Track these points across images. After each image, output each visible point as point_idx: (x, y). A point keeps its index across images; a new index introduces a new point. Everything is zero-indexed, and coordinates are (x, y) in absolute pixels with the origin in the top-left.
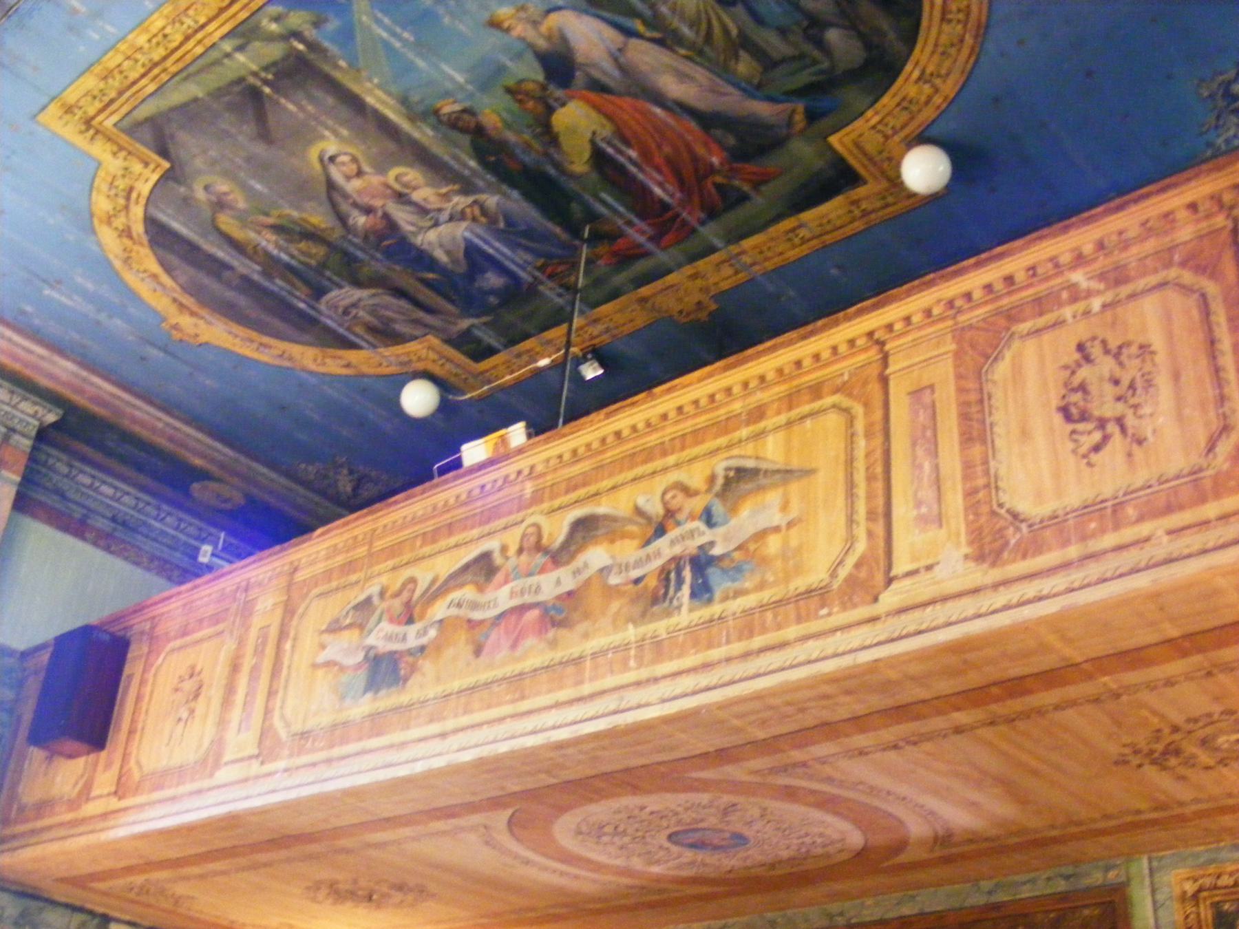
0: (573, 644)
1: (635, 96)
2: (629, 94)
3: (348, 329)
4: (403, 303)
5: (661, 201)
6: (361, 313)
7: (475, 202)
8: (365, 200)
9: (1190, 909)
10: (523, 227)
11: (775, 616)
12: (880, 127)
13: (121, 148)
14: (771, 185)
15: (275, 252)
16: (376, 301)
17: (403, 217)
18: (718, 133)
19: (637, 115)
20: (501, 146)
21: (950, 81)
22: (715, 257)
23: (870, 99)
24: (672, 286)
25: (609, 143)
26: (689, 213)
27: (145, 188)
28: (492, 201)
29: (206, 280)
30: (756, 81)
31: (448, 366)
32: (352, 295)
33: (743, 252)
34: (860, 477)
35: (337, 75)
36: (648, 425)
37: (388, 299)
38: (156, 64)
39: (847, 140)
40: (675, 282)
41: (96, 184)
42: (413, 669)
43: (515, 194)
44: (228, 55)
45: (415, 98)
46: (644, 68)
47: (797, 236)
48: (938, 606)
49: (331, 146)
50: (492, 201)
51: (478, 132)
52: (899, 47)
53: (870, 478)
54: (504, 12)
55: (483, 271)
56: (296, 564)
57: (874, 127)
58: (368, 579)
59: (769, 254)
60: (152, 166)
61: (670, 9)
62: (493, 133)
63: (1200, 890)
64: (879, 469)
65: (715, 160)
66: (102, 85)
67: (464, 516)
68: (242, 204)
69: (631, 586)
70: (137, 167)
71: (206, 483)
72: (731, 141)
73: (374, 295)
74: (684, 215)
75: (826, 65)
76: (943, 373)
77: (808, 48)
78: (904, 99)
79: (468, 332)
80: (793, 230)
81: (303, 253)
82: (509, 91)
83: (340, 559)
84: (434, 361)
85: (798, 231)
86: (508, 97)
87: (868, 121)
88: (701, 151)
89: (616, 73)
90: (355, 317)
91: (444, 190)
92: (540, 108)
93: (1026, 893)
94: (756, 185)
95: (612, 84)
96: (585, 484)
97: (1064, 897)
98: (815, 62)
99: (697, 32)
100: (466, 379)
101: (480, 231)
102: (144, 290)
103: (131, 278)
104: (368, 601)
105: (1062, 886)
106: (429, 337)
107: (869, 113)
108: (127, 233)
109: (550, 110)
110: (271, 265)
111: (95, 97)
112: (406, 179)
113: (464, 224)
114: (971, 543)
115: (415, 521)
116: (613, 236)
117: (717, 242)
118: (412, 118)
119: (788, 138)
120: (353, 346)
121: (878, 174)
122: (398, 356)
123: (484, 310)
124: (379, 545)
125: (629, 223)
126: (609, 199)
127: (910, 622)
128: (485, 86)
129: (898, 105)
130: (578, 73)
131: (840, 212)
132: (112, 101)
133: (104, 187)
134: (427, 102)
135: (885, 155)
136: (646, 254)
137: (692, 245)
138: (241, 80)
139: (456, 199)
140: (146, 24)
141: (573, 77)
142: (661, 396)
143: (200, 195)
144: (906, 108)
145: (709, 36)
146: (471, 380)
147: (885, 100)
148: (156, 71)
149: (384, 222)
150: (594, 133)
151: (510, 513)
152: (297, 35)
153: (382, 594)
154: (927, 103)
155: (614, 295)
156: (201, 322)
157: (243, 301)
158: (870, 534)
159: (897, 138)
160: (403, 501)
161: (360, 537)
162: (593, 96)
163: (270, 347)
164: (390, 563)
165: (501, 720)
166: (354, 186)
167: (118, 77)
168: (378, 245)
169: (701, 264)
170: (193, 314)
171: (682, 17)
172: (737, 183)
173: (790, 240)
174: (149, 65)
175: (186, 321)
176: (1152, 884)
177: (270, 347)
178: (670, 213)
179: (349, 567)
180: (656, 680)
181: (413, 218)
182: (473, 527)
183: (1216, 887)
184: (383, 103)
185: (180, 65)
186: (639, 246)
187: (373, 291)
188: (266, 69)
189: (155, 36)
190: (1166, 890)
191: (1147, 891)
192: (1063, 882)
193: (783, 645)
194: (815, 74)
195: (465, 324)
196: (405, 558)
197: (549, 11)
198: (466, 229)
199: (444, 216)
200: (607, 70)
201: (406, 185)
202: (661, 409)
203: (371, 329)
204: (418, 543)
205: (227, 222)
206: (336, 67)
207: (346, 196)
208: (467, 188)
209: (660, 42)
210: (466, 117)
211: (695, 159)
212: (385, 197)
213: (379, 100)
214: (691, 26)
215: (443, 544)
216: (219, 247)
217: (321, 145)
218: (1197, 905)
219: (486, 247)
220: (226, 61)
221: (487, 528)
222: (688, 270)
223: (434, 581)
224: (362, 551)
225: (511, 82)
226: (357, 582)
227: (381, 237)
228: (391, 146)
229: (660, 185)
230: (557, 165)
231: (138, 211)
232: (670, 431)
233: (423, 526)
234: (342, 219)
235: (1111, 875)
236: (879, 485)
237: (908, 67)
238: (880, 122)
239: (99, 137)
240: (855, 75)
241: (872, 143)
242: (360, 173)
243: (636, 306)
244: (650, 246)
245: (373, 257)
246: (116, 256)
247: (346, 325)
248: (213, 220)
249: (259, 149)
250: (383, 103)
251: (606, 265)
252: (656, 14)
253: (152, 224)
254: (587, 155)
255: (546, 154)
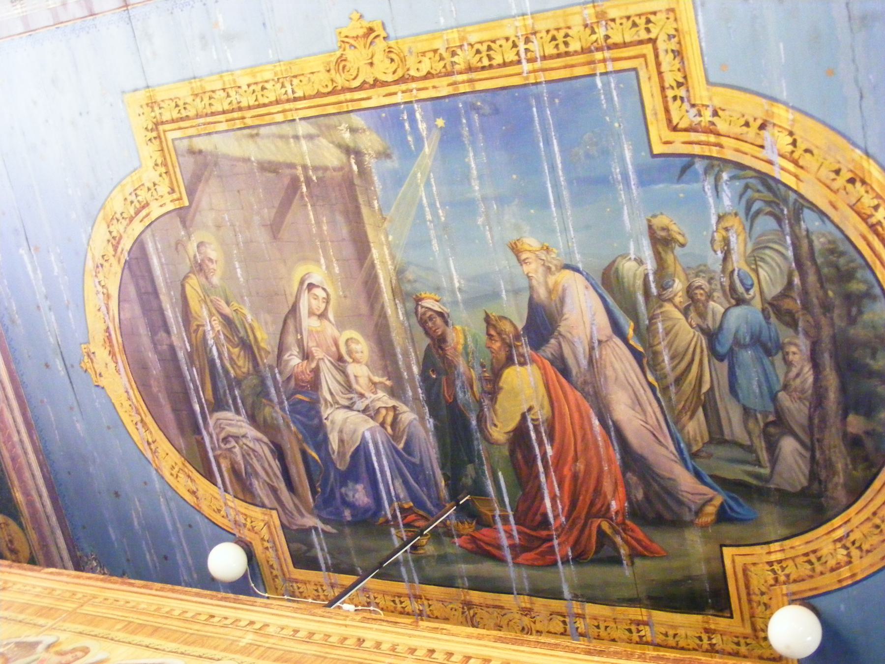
1: (586, 395)
2: (582, 391)
3: (216, 458)
4: (275, 465)
5: (545, 515)
6: (237, 450)
7: (394, 408)
8: (310, 344)
10: (417, 461)
12: (776, 567)
13: (165, 165)
14: (648, 563)
15: (211, 342)
16: (257, 447)
17: (329, 381)
18: (633, 479)
19: (576, 416)
20: (449, 367)
21: (868, 559)
22: (556, 605)
23: (783, 531)
24: (502, 608)
25: (536, 428)
26: (559, 544)
27: (156, 211)
28: (408, 416)
29: (143, 331)
30: (695, 449)
31: (271, 553)
32: (241, 427)
33: (582, 616)
35: (365, 211)
36: (393, 649)
37: (266, 451)
38: (240, 109)
39: (740, 561)
40: (507, 606)
41: (124, 182)
43: (430, 423)
44: (296, 137)
45: (410, 275)
46: (609, 372)
47: (639, 631)
49: (317, 275)
50: (408, 416)
51: (439, 341)
52: (841, 495)
54: (531, 242)
55: (357, 481)
56: (10, 585)
57: (770, 563)
58: (52, 628)
59: (603, 633)
60: (175, 196)
61: (665, 329)
62: (450, 353)
65: (614, 505)
66: (189, 100)
67: (174, 628)
68: (215, 280)
70: (164, 189)
71: (10, 521)
72: (640, 495)
73: (258, 440)
74: (556, 542)
75: (765, 471)
77: (760, 445)
78: (814, 552)
79: (307, 531)
80: (638, 623)
81: (231, 359)
82: (488, 319)
83: (46, 602)
84: (263, 539)
85: (641, 627)
86: (484, 325)
87: (769, 553)
88: (607, 486)
89: (584, 362)
90: (230, 450)
91: (376, 379)
92: (503, 355)
94: (634, 554)
95: (574, 371)
98: (758, 463)
99: (674, 368)
100: (276, 576)
101: (379, 439)
102: (93, 301)
103: (90, 284)
104: (33, 646)
106: (274, 513)
107: (775, 546)
108: (115, 242)
109: (509, 361)
110: (199, 351)
111: (177, 106)
112: (353, 346)
113: (372, 423)
115: (135, 610)
116: (483, 522)
117: (567, 594)
118: (396, 292)
119: (691, 523)
120: (209, 476)
121: (747, 616)
122: (238, 513)
123: (335, 520)
124: (88, 609)
125: (505, 519)
128: (471, 303)
129: (806, 555)
130: (553, 341)
131: (690, 633)
132: (188, 118)
133: (129, 189)
134: (418, 285)
135: (765, 599)
136: (501, 560)
137: (544, 577)
138: (292, 166)
139: (381, 394)
140: (257, 69)
141: (547, 341)
142: (423, 630)
143: (192, 248)
144: (810, 562)
145: (679, 381)
146: (279, 581)
147: (796, 541)
148: (236, 115)
149: (312, 375)
150: (530, 409)
151: (215, 648)
152: (358, 154)
153: (49, 647)
154: (832, 570)
155: (448, 582)
156: (112, 365)
157: (156, 369)
159: (785, 589)
160: (138, 587)
161: (80, 595)
162: (551, 371)
163: (147, 429)
164: (81, 628)
166: (309, 323)
167: (206, 100)
168: (293, 394)
169: (539, 602)
170: (112, 353)
171: (670, 345)
172: (618, 540)
173: (630, 631)
174: (235, 106)
175: (102, 355)
177: (147, 429)
178: (544, 533)
179: (46, 612)
181: (335, 388)
182: (174, 641)
184: (383, 263)
185: (257, 122)
186: (499, 547)
187: (259, 435)
188: (315, 169)
189: (256, 83)
194: (749, 474)
195: (310, 521)
196: (97, 631)
197: (567, 267)
198: (370, 429)
199: (361, 405)
200: (578, 362)
201: (350, 353)
202: (413, 642)
203: (235, 471)
204: (119, 626)
205: (193, 287)
206: (370, 205)
207: (298, 330)
208: (395, 392)
209: (637, 356)
210: (439, 321)
211: (598, 490)
212: (328, 353)
213: (382, 255)
214: (672, 358)
215: (137, 638)
216: (173, 307)
217: (311, 268)
219: (374, 459)
220: (292, 140)
221: (183, 648)
222: (524, 601)
224: (69, 606)
225: (494, 313)
226: (42, 626)
227: (299, 389)
228: (364, 309)
229: (553, 499)
230: (481, 419)
231: (137, 227)
233: (136, 616)
234: (281, 349)
237: (837, 521)
238: (779, 562)
239: (157, 142)
240: (784, 498)
241: (760, 577)
242: (323, 316)
243: (458, 605)
244: (508, 555)
245: (281, 403)
246: (93, 258)
247: (218, 452)
248: (186, 277)
249: (262, 237)
250: (383, 263)
251: (460, 546)
252: (649, 328)
253: (139, 250)
254: (512, 425)
255: (480, 404)
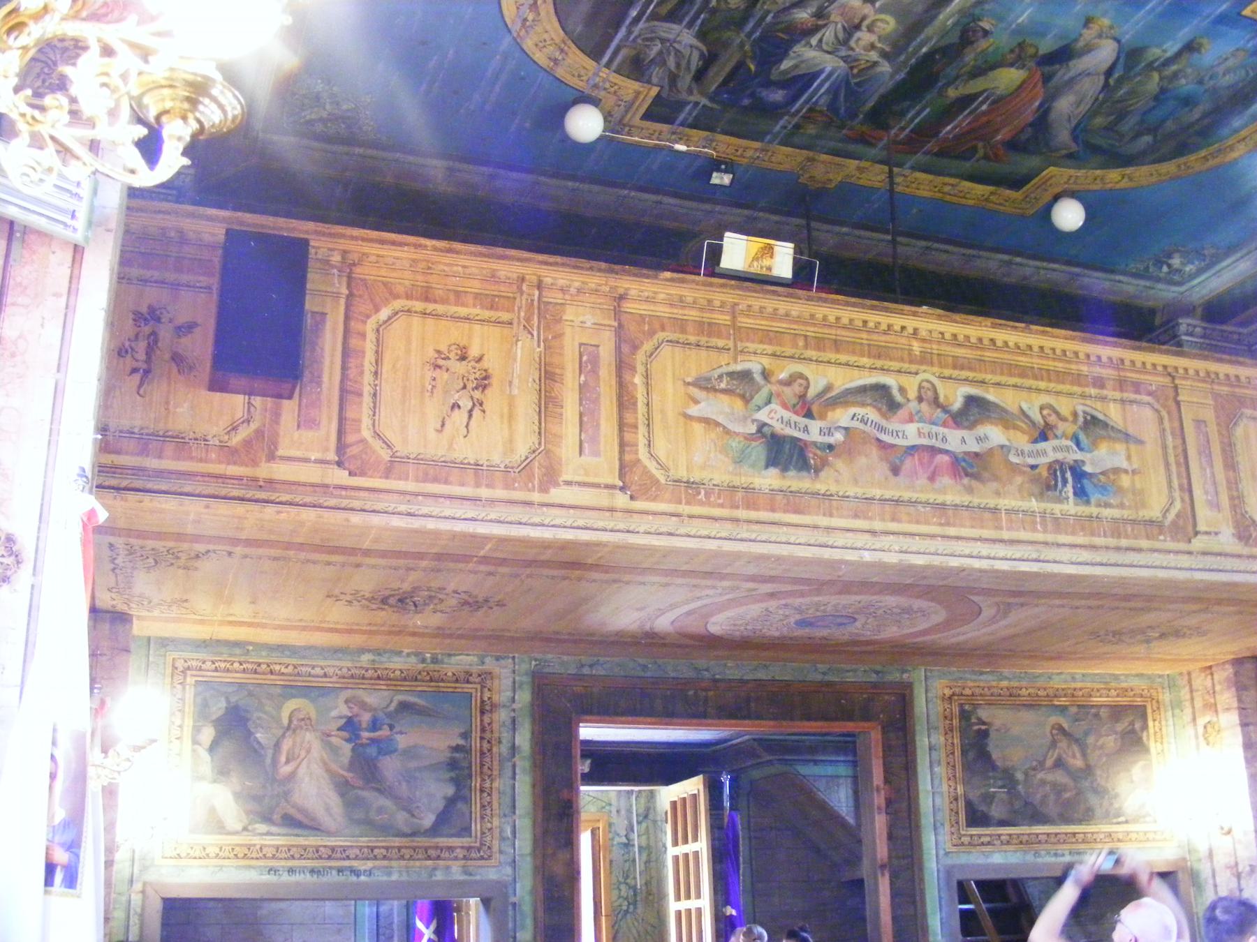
0: (985, 496)
9: (947, 706)
11: (1133, 530)
34: (1172, 459)
42: (824, 463)
48: (1223, 558)
53: (1178, 464)
63: (954, 694)
64: (1182, 460)
69: (1029, 469)
76: (1209, 415)
93: (850, 678)
96: (971, 369)
97: (875, 685)
105: (873, 678)
114: (1235, 528)
126: (925, 113)
127: (1210, 562)
158: (1183, 500)
165: (933, 536)
176: (926, 686)
180: (1059, 545)
183: (962, 695)
190: (934, 691)
191: (923, 690)
192: (875, 676)
193: (1139, 550)
218: (951, 703)
223: (828, 388)
232: (1036, 362)
233: (803, 328)
235: (905, 676)
236: (1183, 469)
